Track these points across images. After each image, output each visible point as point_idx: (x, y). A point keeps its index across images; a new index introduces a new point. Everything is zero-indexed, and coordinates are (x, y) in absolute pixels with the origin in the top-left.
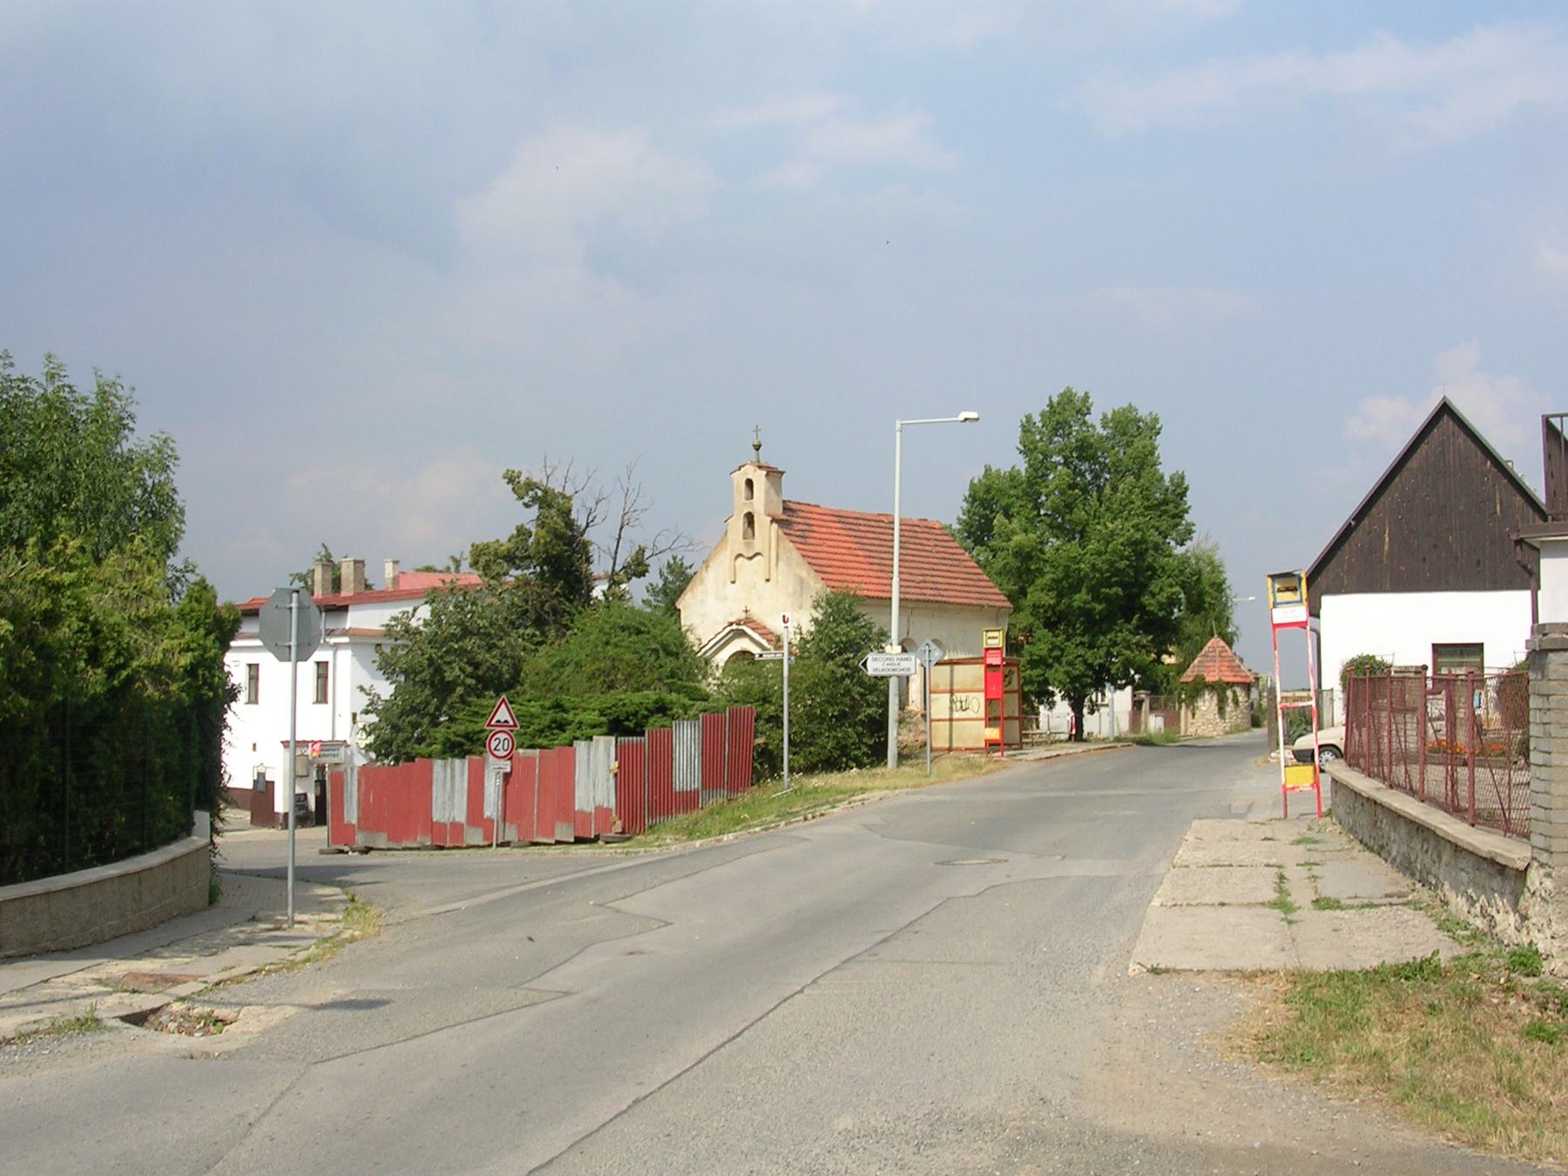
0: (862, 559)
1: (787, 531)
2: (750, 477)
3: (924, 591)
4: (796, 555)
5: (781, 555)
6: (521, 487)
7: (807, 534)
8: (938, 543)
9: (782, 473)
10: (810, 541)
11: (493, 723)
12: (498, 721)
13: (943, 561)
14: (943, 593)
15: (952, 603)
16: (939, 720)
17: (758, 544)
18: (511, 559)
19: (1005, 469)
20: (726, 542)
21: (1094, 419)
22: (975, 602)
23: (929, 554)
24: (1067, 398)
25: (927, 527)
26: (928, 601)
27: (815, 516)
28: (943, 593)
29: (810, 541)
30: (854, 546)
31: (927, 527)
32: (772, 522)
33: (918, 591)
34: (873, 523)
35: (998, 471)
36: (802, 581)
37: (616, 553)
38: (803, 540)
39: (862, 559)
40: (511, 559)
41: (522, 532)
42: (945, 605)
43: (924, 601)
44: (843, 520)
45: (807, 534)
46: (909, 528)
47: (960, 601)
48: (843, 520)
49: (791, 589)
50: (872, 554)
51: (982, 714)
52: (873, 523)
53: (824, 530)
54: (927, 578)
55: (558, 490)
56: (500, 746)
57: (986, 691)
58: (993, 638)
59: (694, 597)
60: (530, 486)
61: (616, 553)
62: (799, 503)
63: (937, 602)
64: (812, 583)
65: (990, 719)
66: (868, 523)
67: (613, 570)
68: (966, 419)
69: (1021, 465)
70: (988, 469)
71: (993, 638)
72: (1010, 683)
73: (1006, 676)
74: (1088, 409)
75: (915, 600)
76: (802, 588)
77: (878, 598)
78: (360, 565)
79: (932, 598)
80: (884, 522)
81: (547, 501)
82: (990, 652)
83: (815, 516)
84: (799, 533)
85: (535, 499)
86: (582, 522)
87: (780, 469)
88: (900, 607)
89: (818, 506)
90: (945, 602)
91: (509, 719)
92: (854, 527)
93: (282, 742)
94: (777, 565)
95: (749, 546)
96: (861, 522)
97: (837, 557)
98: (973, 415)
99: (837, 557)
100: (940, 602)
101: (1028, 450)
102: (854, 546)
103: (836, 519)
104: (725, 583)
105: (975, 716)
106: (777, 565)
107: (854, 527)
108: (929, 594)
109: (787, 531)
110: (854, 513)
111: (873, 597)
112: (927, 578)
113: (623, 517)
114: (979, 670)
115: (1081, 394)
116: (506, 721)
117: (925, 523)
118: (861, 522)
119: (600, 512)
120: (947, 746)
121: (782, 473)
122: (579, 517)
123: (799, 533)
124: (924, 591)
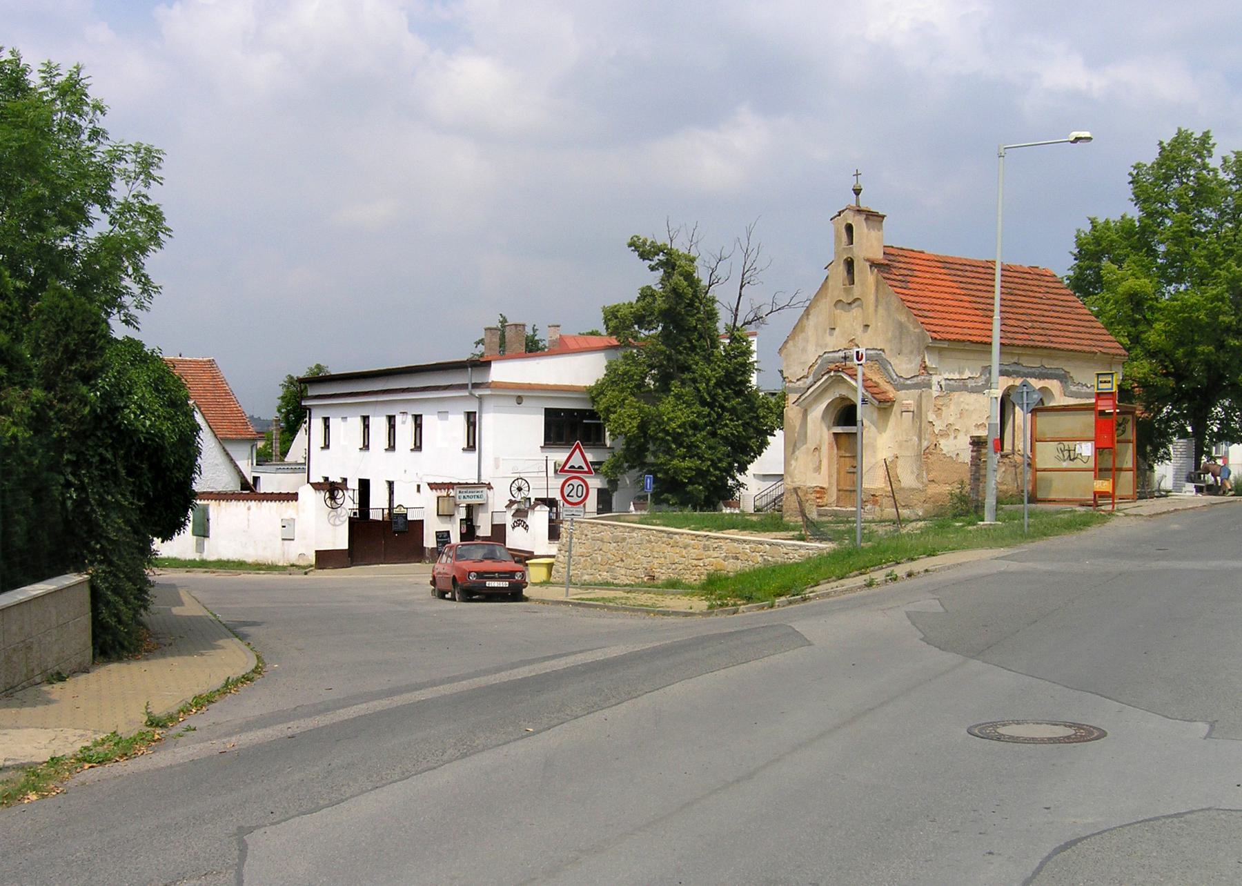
0: (967, 305)
1: (886, 275)
2: (850, 222)
3: (1032, 337)
4: (895, 301)
5: (880, 299)
6: (644, 251)
7: (909, 279)
8: (1048, 290)
9: (883, 217)
10: (910, 285)
11: (566, 468)
12: (572, 467)
13: (1054, 308)
14: (1052, 339)
15: (1063, 350)
16: (1044, 470)
17: (857, 291)
18: (641, 320)
19: (1115, 217)
20: (827, 289)
21: (1214, 162)
22: (1086, 349)
23: (1039, 301)
24: (1182, 140)
25: (1038, 274)
26: (1036, 347)
27: (918, 261)
28: (1052, 339)
29: (910, 285)
30: (958, 291)
31: (1038, 274)
32: (871, 266)
33: (1025, 336)
34: (980, 270)
35: (1107, 222)
36: (901, 326)
37: (737, 309)
38: (903, 285)
39: (967, 305)
40: (641, 320)
41: (647, 294)
42: (1053, 352)
43: (1032, 347)
44: (948, 265)
45: (909, 279)
46: (1019, 275)
47: (1071, 347)
48: (948, 265)
49: (890, 334)
50: (979, 300)
51: (1091, 464)
52: (980, 270)
53: (928, 275)
54: (1035, 325)
55: (683, 251)
56: (573, 493)
57: (1096, 440)
58: (1105, 382)
59: (795, 346)
60: (658, 250)
61: (737, 309)
62: (902, 249)
63: (1045, 348)
64: (911, 327)
65: (1100, 470)
66: (975, 269)
67: (734, 325)
68: (1077, 139)
69: (1134, 213)
70: (1093, 222)
71: (1105, 382)
72: (1124, 432)
73: (1120, 425)
74: (1209, 151)
75: (1022, 346)
76: (901, 333)
77: (981, 343)
78: (521, 328)
79: (1041, 344)
80: (989, 267)
81: (670, 263)
82: (1102, 397)
83: (918, 261)
84: (900, 278)
85: (661, 264)
86: (705, 283)
87: (881, 213)
88: (1001, 353)
89: (923, 252)
90: (1054, 348)
91: (584, 466)
92: (960, 273)
93: (429, 484)
94: (876, 311)
95: (848, 291)
96: (968, 268)
97: (940, 302)
98: (1087, 134)
99: (940, 302)
100: (1050, 348)
101: (1142, 196)
102: (958, 291)
103: (939, 265)
104: (825, 330)
105: (1084, 466)
106: (876, 311)
107: (960, 273)
108: (1038, 340)
109: (886, 275)
110: (960, 259)
111: (977, 343)
112: (1035, 325)
113: (743, 275)
114: (1090, 419)
115: (1198, 135)
116: (580, 467)
117: (1037, 271)
118: (968, 268)
119: (721, 272)
120: (1039, 465)
121: (883, 217)
122: (702, 275)
123: (900, 278)
124: (1032, 337)
